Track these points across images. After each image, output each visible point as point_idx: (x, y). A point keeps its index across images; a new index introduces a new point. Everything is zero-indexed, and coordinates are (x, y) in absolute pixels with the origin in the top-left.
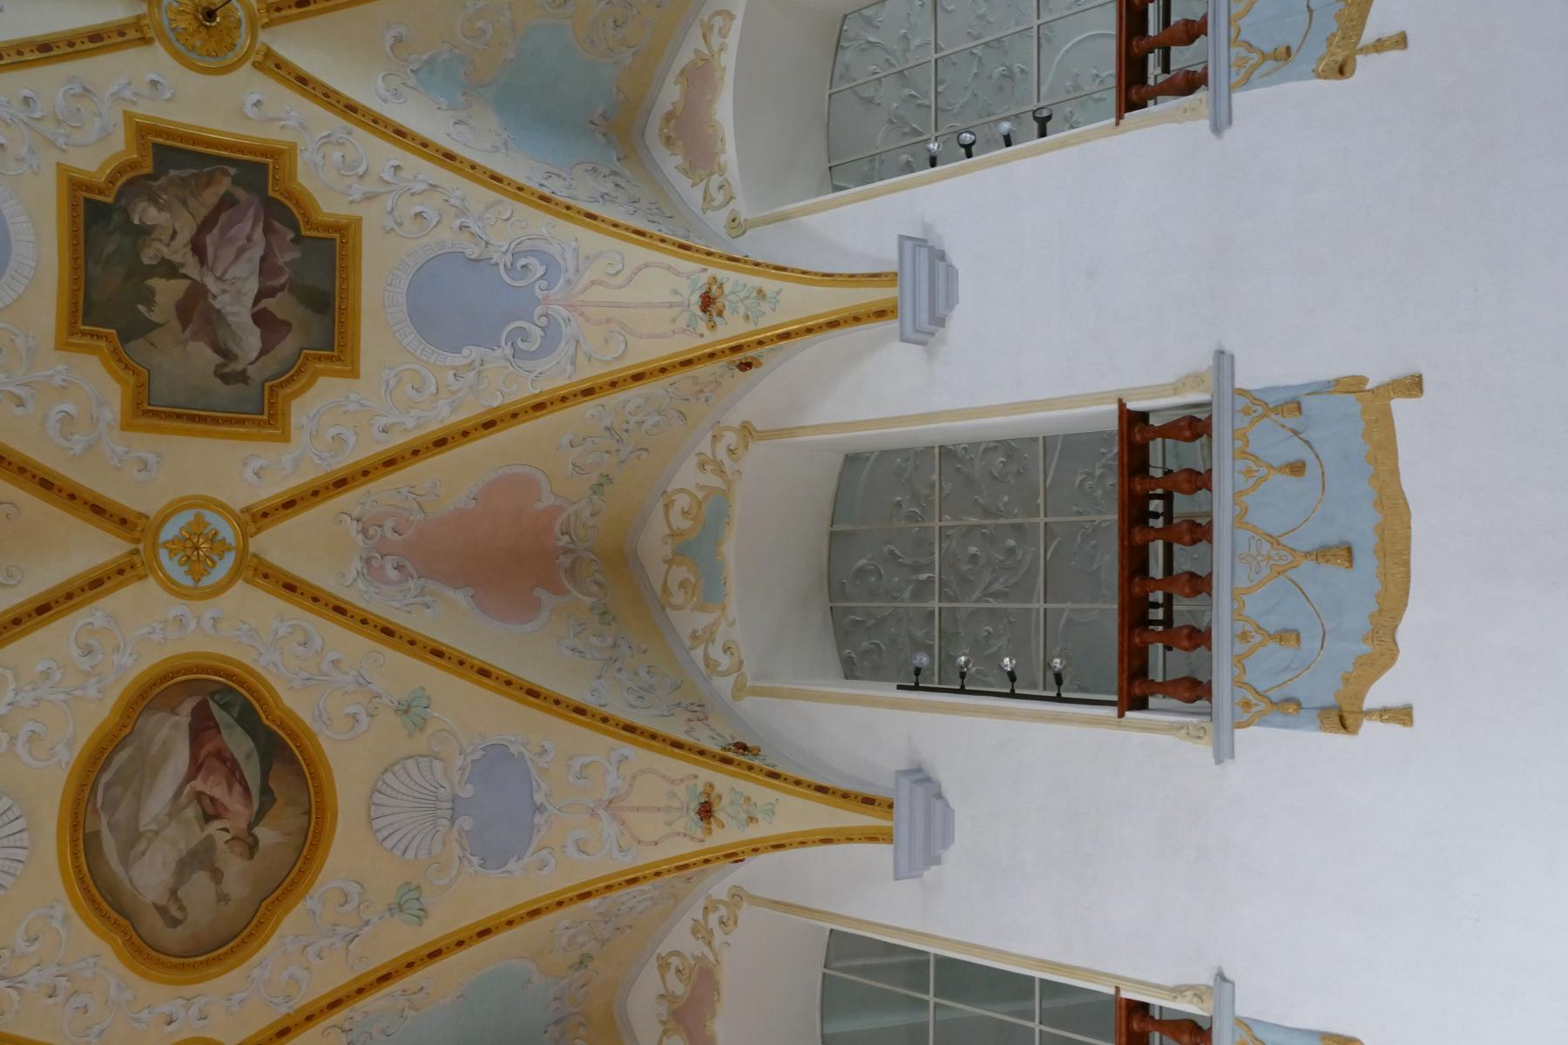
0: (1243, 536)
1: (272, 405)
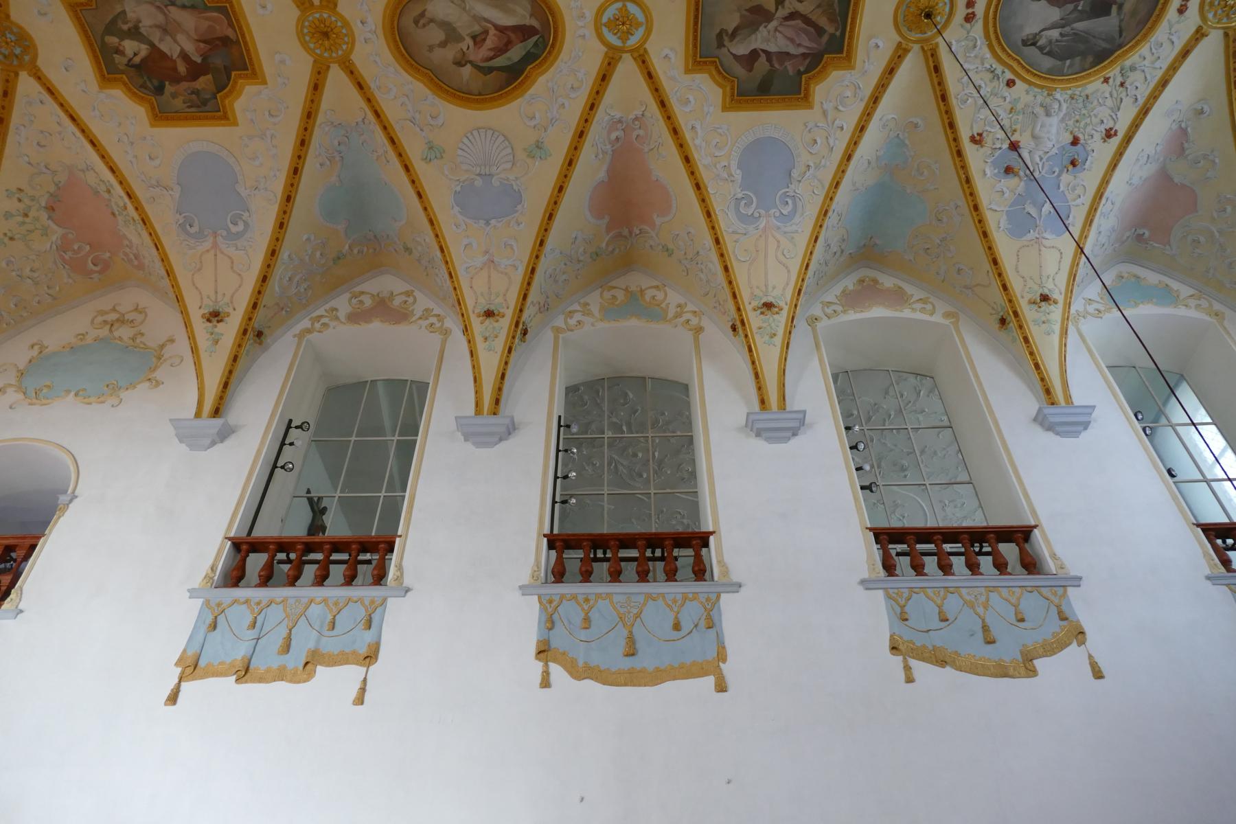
0: (641, 599)
1: (705, 63)
